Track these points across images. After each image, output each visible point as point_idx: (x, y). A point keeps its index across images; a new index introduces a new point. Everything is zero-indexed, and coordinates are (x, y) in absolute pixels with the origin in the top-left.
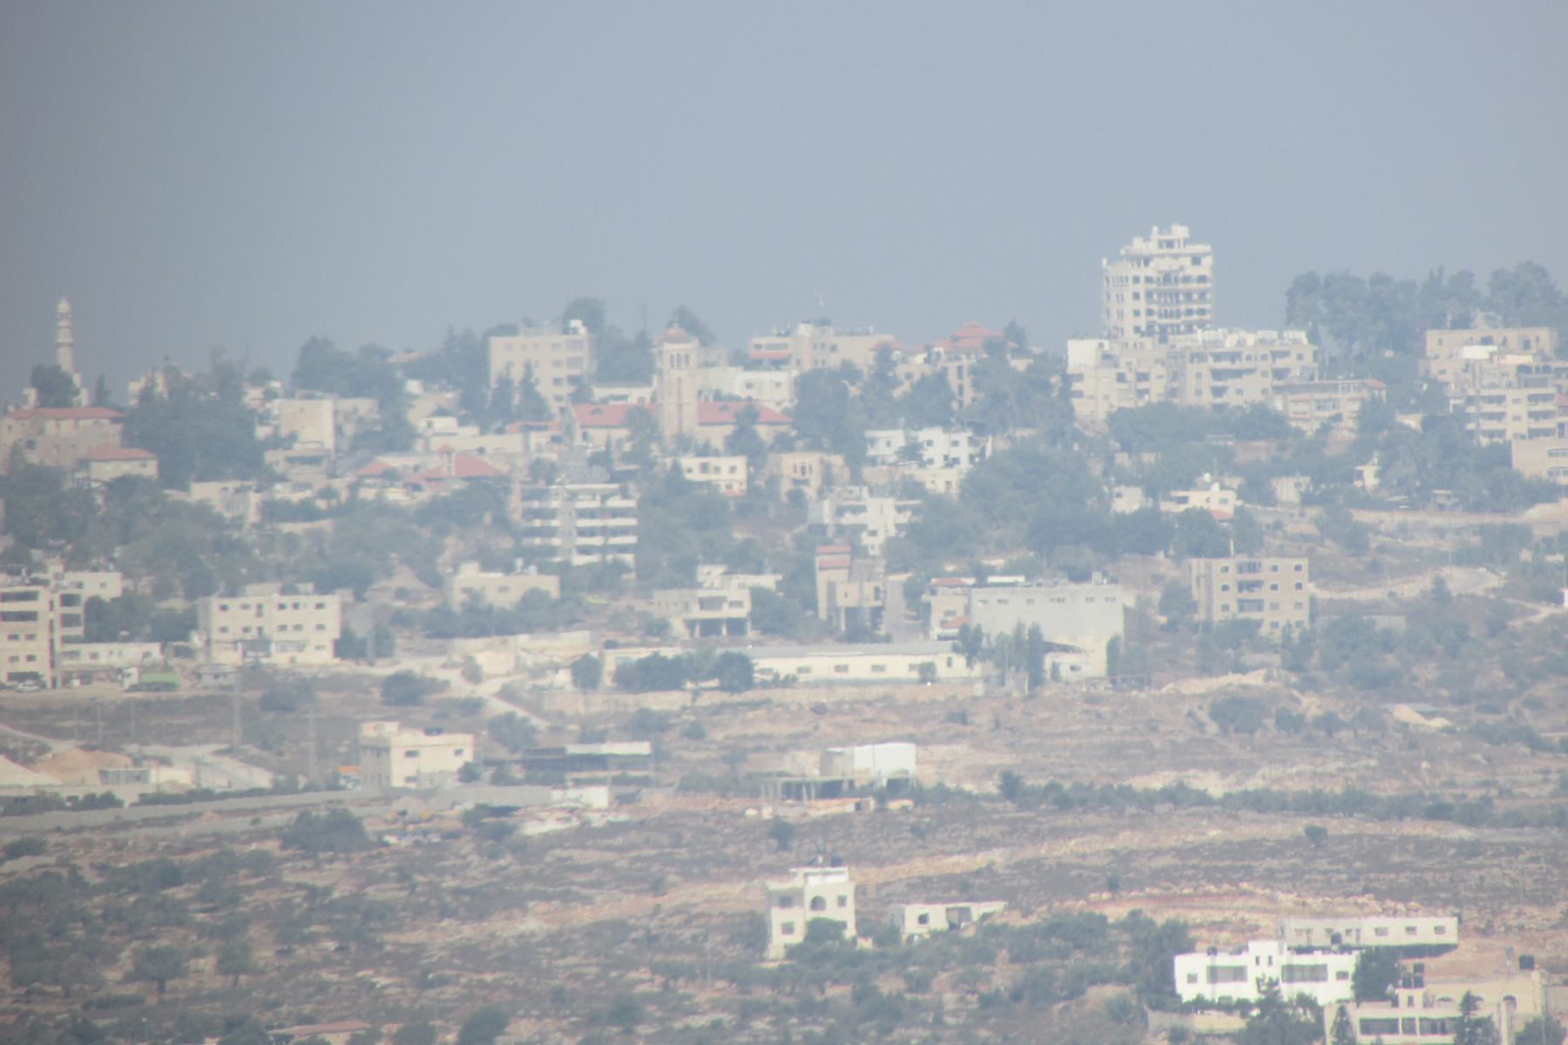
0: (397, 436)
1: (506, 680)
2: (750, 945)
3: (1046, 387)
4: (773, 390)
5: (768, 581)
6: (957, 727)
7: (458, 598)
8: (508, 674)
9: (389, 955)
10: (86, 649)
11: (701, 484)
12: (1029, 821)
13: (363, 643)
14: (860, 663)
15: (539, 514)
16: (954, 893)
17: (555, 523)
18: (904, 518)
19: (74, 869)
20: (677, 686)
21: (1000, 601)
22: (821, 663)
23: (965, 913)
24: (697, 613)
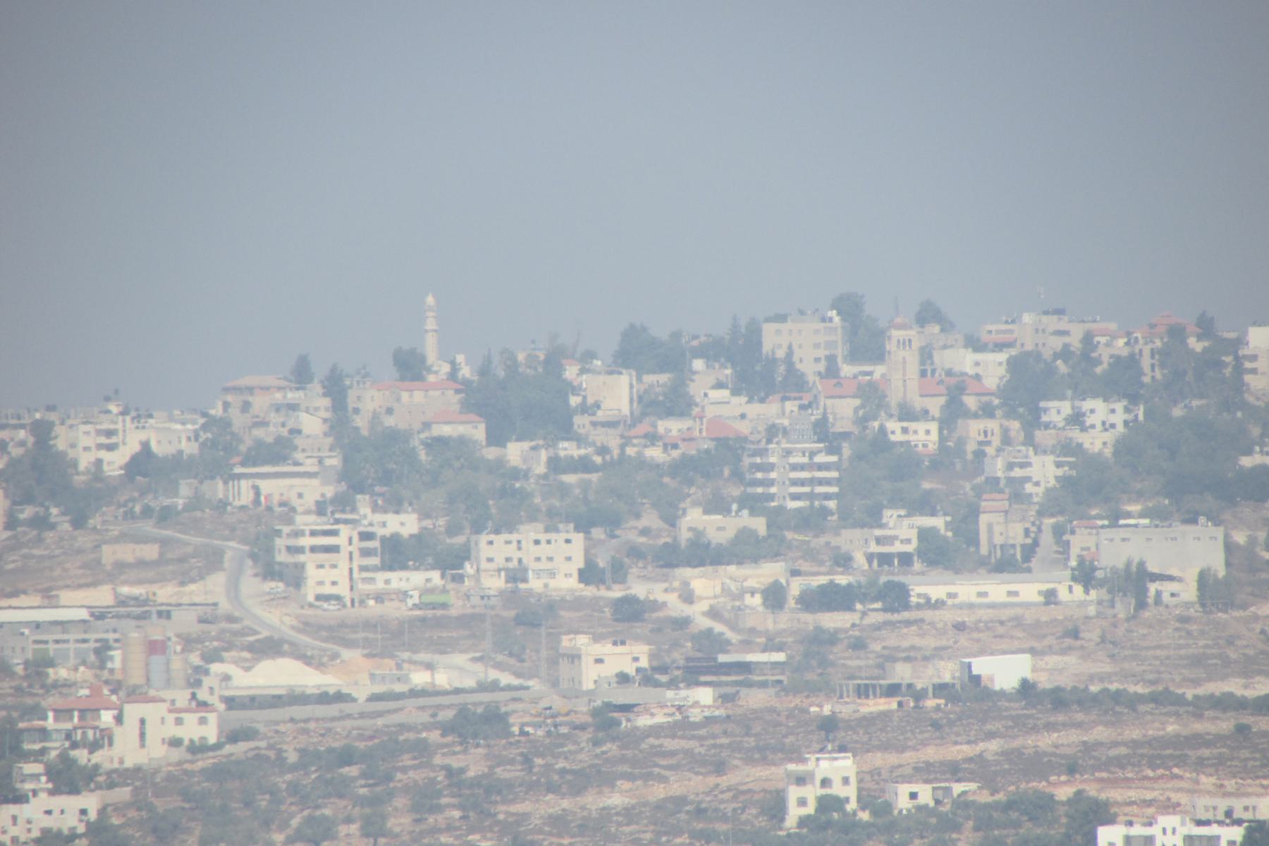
0: (676, 402)
1: (712, 602)
2: (773, 817)
3: (1220, 365)
4: (992, 369)
5: (938, 522)
6: (1069, 641)
7: (685, 535)
8: (715, 597)
9: (498, 822)
10: (381, 577)
11: (901, 443)
12: (1029, 717)
13: (603, 571)
14: (997, 590)
15: (760, 468)
16: (948, 776)
17: (773, 475)
18: (1060, 472)
19: (280, 752)
20: (850, 608)
21: (1124, 540)
22: (967, 589)
23: (948, 790)
24: (874, 548)
